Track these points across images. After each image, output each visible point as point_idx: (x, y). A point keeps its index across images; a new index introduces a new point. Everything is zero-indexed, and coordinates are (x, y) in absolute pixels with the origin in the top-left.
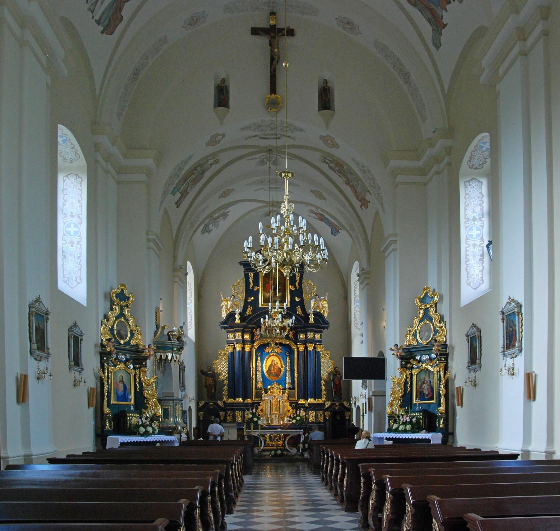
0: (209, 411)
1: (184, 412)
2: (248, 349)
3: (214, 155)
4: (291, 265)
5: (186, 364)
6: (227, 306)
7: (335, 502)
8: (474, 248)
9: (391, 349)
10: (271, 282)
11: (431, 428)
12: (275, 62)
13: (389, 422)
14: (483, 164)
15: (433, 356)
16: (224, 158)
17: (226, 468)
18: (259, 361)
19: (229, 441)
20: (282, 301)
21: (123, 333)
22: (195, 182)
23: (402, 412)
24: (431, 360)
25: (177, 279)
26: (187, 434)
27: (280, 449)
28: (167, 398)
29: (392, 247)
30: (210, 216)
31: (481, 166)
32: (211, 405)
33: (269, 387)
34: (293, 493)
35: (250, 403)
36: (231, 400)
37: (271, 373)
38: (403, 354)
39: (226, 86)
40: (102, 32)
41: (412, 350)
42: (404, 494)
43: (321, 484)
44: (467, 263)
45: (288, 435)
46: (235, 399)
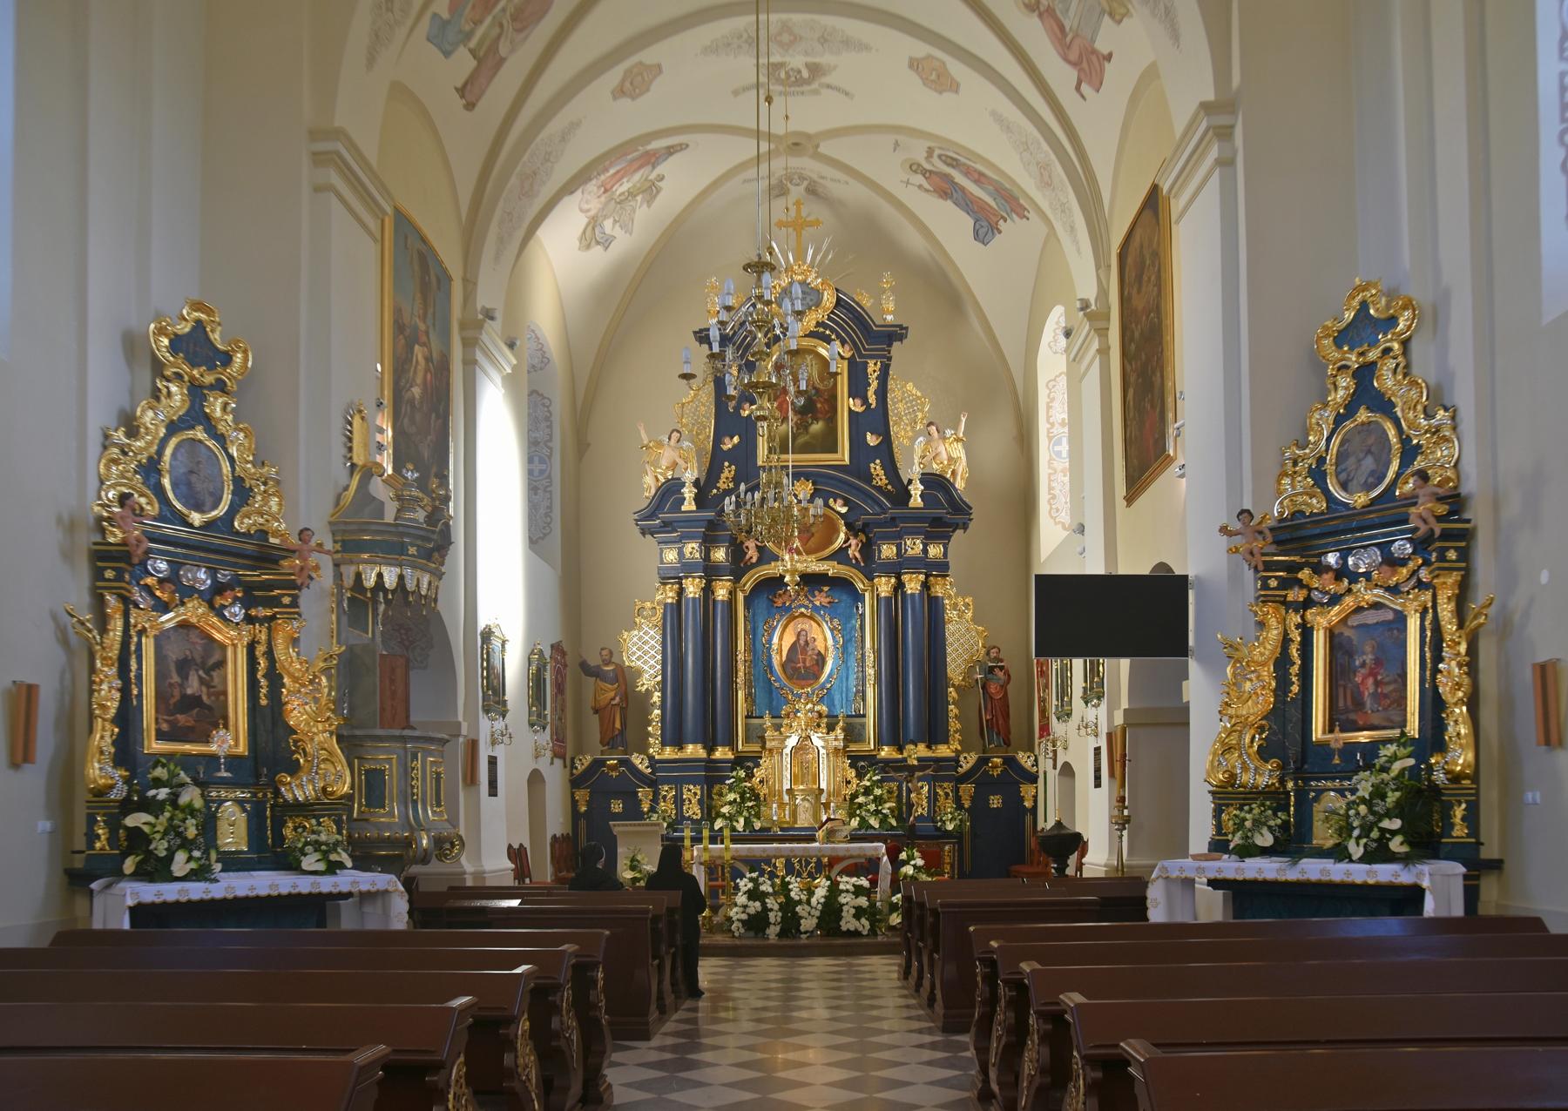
32: (613, 768)
36: (669, 753)
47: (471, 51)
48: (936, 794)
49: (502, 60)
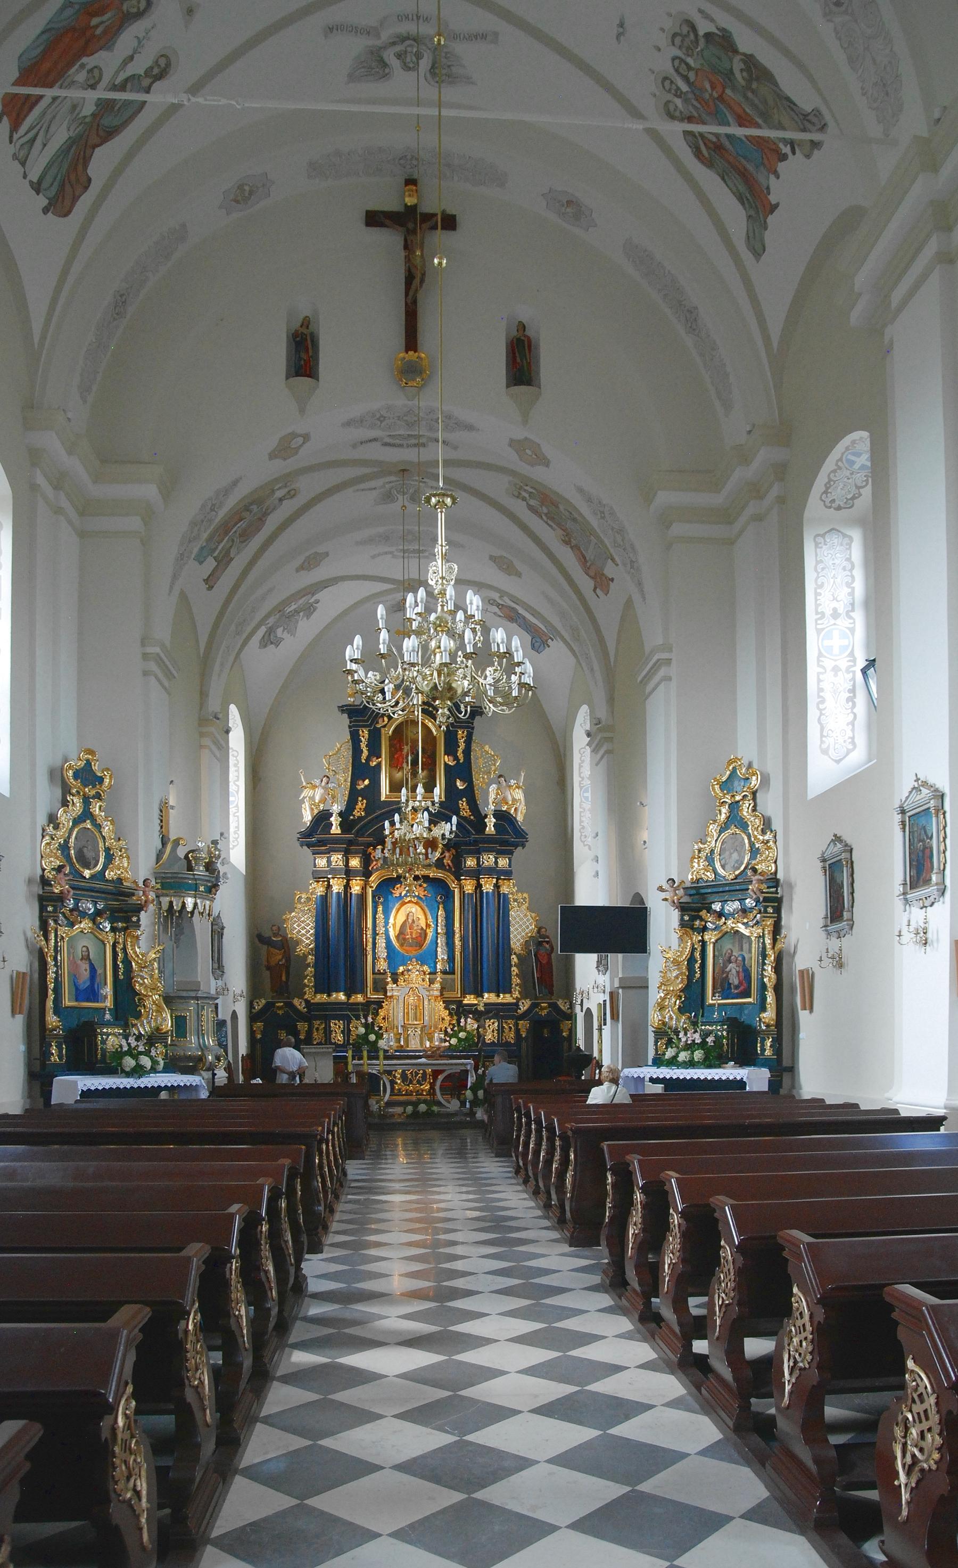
0: (275, 1019)
1: (221, 1024)
2: (358, 888)
3: (286, 479)
4: (451, 699)
5: (225, 921)
6: (312, 798)
7: (547, 1223)
8: (836, 675)
9: (661, 889)
10: (406, 749)
11: (746, 1058)
12: (416, 282)
13: (656, 1044)
14: (853, 498)
15: (749, 902)
16: (308, 486)
17: (307, 1152)
18: (380, 915)
19: (316, 1085)
20: (429, 788)
21: (89, 854)
22: (245, 536)
23: (683, 1021)
24: (744, 911)
25: (206, 741)
26: (229, 1069)
27: (425, 1102)
28: (184, 994)
29: (662, 672)
30: (279, 609)
31: (850, 503)
33: (401, 969)
34: (453, 1198)
35: (362, 1004)
36: (322, 998)
37: (404, 939)
38: (686, 899)
39: (312, 334)
40: (45, 211)
41: (703, 891)
42: (717, 1220)
43: (514, 1181)
44: (821, 706)
45: (441, 1072)
46: (329, 995)
47: (215, 558)
48: (503, 1027)
49: (232, 559)
